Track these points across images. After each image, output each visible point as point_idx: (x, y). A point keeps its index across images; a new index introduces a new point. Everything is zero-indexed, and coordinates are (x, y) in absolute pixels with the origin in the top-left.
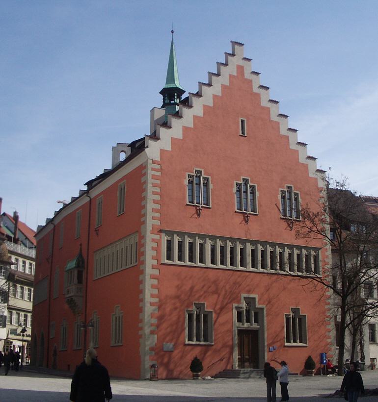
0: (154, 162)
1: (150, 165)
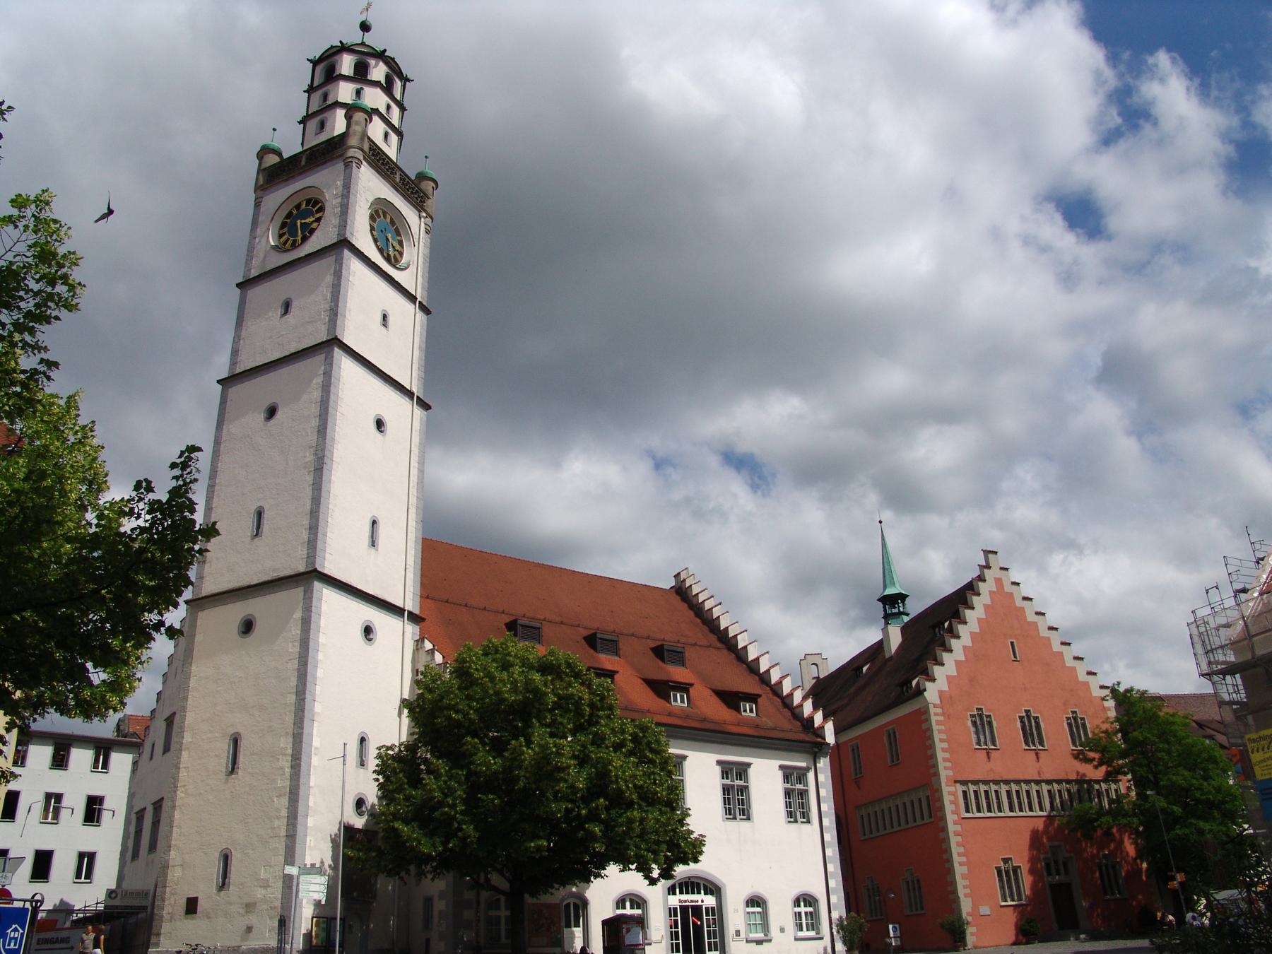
0: (935, 706)
1: (932, 710)
